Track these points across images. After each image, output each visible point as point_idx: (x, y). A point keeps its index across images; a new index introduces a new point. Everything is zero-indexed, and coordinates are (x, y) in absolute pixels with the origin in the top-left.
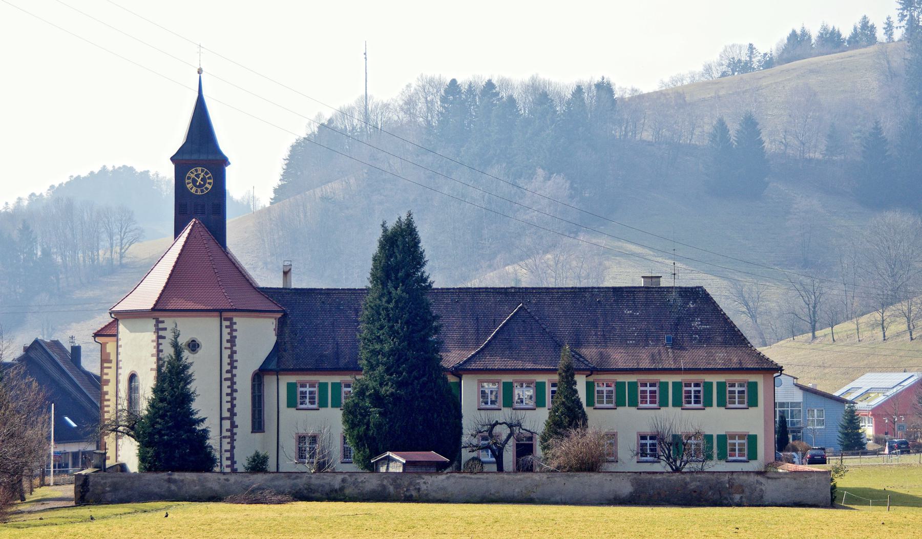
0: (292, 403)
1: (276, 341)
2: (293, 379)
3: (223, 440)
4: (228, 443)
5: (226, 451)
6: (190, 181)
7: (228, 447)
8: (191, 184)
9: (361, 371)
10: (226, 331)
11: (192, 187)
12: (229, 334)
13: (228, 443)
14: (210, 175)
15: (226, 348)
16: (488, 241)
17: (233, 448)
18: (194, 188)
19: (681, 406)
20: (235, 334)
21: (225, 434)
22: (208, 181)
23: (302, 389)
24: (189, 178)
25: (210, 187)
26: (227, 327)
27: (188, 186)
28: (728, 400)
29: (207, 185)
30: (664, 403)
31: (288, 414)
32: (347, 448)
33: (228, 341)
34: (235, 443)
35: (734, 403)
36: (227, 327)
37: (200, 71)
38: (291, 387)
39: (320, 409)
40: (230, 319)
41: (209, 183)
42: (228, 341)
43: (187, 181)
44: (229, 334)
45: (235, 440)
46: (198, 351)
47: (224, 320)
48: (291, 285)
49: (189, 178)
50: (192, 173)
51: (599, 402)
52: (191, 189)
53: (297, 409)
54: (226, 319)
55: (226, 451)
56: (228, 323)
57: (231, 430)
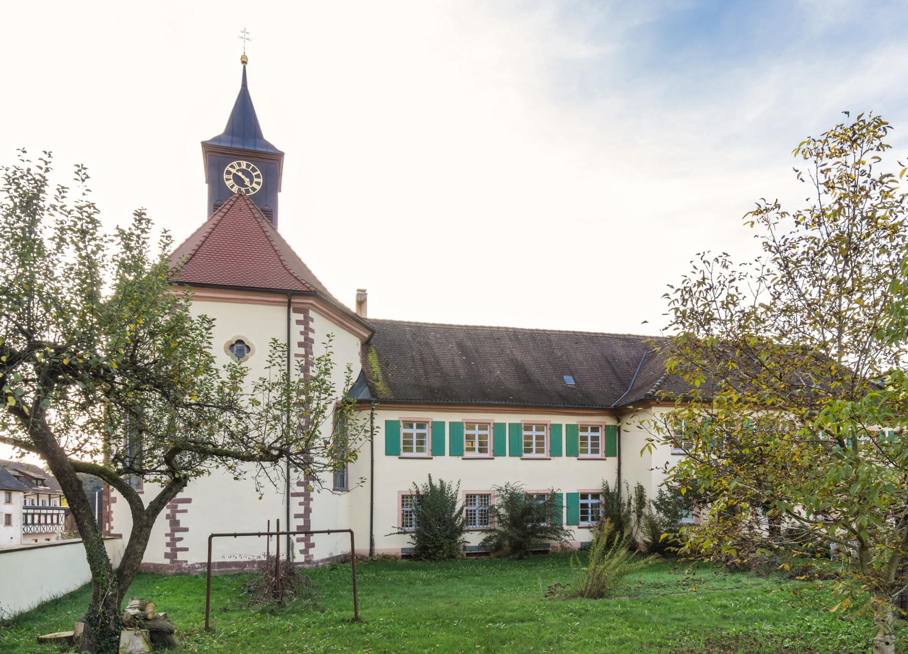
0: (392, 450)
1: (362, 370)
2: (395, 415)
3: (292, 499)
4: (300, 504)
5: (297, 516)
6: (231, 177)
7: (301, 510)
8: (232, 181)
9: (674, 401)
10: (296, 329)
11: (233, 185)
12: (302, 333)
13: (300, 504)
14: (259, 172)
15: (296, 355)
16: (151, 461)
17: (308, 511)
18: (236, 186)
19: (462, 455)
20: (311, 335)
21: (295, 489)
22: (256, 180)
23: (470, 432)
24: (229, 173)
25: (258, 188)
26: (298, 322)
27: (227, 183)
28: (402, 446)
29: (254, 185)
30: (438, 450)
31: (386, 465)
32: (471, 511)
33: (300, 345)
34: (312, 505)
35: (411, 450)
36: (298, 322)
37: (244, 62)
38: (391, 427)
39: (434, 457)
40: (304, 311)
41: (258, 183)
42: (300, 345)
43: (225, 176)
44: (302, 333)
45: (312, 500)
46: (247, 358)
47: (294, 312)
48: (366, 315)
49: (229, 173)
50: (232, 167)
51: (405, 450)
52: (232, 187)
53: (400, 458)
54: (297, 311)
55: (297, 516)
56: (301, 317)
57: (305, 484)
